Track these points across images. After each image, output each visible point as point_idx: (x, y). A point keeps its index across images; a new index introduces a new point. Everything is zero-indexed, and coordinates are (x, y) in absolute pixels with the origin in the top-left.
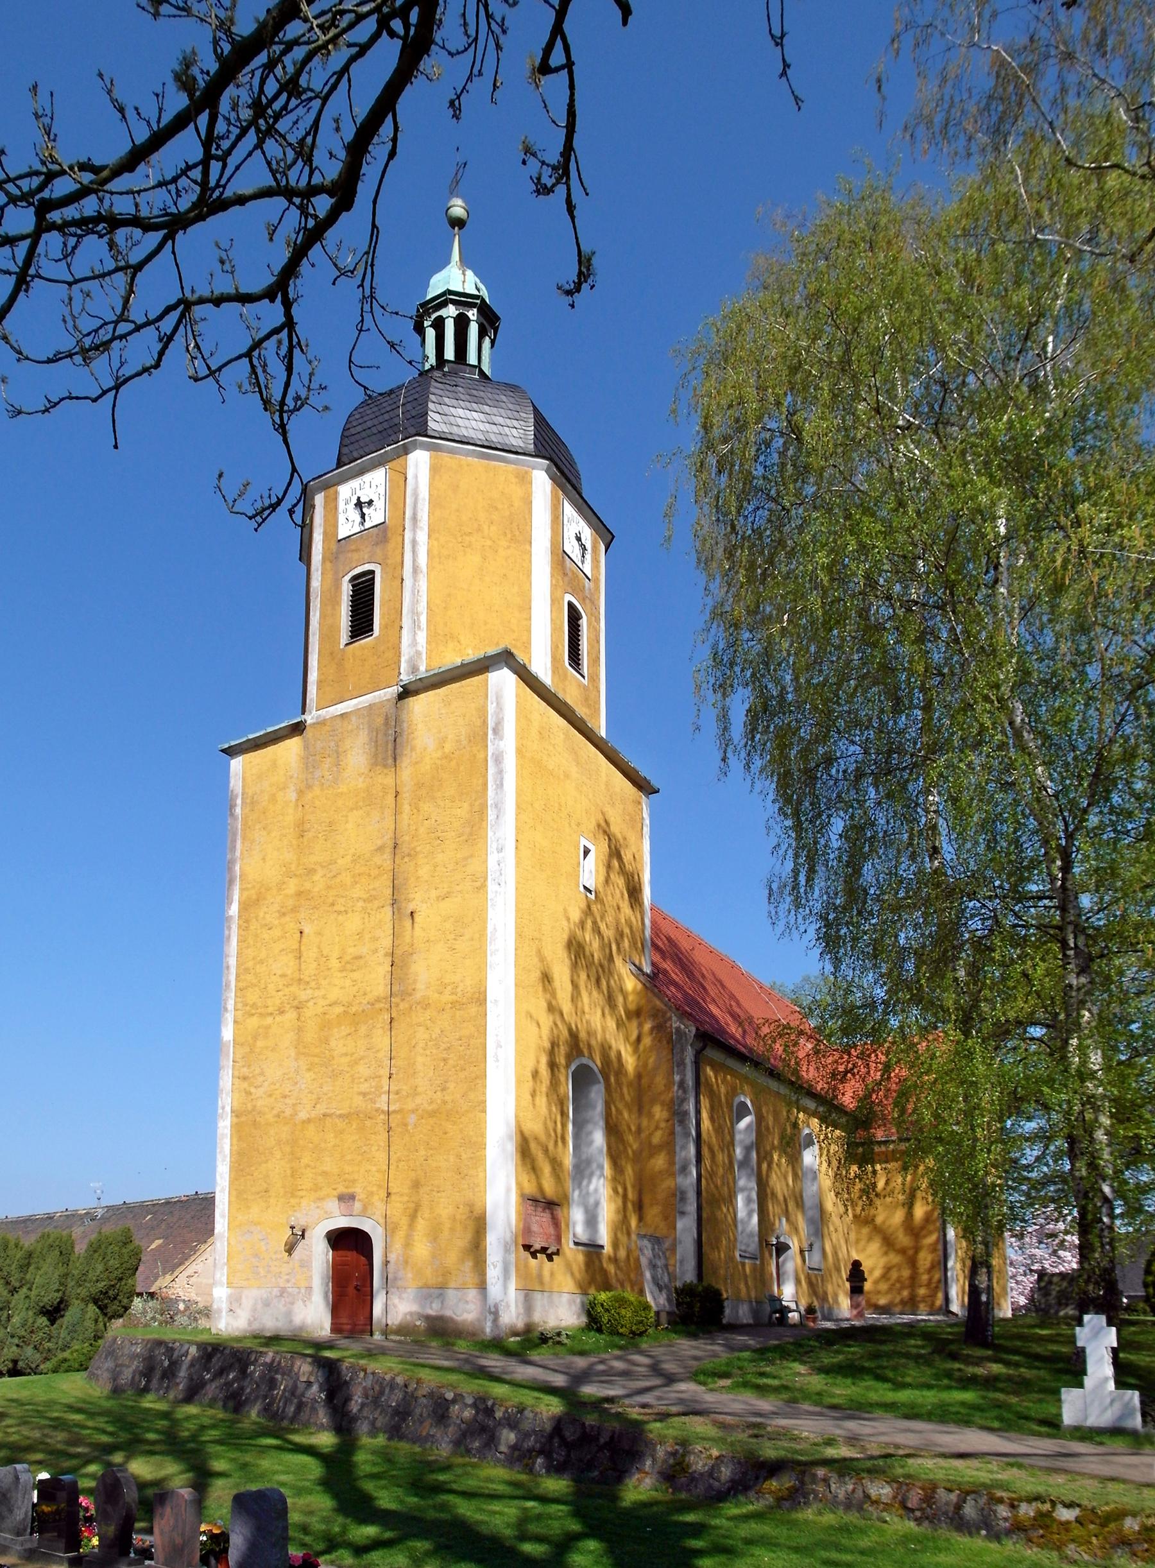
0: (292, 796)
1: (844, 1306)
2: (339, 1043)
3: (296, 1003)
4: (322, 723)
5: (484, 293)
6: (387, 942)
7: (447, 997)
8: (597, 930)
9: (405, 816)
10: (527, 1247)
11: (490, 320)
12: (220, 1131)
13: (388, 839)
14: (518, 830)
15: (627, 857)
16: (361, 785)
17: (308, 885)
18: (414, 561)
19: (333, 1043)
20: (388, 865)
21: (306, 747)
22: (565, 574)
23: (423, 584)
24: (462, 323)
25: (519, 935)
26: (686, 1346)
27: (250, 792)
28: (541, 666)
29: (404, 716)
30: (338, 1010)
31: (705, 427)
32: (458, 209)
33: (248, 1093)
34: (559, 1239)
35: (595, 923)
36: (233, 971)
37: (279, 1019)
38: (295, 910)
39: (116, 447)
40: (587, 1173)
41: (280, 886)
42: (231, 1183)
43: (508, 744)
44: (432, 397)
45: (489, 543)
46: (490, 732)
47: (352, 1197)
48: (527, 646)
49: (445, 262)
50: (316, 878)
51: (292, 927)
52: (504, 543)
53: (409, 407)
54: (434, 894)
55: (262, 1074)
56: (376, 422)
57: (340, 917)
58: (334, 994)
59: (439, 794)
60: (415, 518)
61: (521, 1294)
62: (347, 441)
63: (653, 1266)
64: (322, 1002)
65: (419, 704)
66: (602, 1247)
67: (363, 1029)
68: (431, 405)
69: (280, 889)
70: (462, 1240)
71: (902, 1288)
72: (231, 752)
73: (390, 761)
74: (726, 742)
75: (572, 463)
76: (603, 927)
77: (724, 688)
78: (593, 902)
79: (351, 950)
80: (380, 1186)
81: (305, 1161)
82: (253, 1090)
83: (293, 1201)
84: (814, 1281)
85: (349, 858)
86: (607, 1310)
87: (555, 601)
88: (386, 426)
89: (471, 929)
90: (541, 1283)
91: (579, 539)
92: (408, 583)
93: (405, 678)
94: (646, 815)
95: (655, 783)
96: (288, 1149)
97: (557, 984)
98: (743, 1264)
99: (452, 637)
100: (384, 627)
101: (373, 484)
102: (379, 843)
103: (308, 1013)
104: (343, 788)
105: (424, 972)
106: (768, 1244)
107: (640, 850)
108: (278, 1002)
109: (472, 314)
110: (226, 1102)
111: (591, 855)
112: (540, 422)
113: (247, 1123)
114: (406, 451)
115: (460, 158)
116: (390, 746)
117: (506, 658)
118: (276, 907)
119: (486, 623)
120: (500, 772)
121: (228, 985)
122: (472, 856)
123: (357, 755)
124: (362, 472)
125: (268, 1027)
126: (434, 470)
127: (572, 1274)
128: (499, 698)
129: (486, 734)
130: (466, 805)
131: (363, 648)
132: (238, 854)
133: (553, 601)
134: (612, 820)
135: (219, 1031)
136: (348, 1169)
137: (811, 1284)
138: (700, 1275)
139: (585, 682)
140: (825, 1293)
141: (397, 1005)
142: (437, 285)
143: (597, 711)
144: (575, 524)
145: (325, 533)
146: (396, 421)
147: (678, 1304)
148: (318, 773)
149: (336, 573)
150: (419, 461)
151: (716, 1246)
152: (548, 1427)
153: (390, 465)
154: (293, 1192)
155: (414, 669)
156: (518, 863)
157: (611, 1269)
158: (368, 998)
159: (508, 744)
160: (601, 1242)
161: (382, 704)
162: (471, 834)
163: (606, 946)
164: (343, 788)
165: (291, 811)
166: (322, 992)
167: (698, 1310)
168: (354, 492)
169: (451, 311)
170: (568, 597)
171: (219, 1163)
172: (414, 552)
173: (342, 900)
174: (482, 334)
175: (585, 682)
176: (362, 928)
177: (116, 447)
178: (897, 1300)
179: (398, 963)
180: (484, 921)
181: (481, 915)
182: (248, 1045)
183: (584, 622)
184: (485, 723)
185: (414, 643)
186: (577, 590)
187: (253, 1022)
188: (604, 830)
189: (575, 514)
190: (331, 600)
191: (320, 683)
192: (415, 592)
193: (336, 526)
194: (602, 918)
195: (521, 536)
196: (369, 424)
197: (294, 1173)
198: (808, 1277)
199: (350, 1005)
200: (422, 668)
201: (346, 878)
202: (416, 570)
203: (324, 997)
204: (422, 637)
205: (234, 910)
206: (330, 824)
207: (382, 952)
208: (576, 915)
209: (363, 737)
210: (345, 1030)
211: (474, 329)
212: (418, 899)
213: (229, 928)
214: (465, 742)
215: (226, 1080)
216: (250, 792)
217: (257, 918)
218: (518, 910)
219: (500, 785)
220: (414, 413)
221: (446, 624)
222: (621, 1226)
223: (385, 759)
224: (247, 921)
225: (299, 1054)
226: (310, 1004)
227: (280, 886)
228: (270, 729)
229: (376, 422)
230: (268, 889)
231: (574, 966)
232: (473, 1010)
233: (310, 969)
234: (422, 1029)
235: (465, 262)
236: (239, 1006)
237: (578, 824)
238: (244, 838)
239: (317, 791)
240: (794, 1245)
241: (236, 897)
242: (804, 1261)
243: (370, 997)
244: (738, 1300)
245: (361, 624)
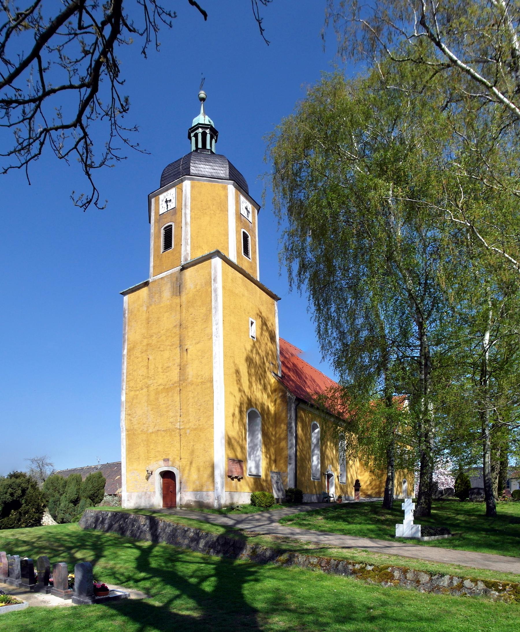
0: (145, 308)
1: (352, 495)
2: (162, 399)
3: (147, 385)
4: (154, 281)
5: (212, 123)
6: (178, 361)
7: (199, 380)
8: (258, 353)
9: (184, 314)
10: (229, 477)
11: (214, 133)
12: (122, 437)
13: (178, 323)
14: (224, 316)
15: (269, 324)
16: (168, 303)
17: (150, 342)
18: (186, 220)
19: (160, 400)
20: (178, 332)
21: (149, 291)
22: (241, 222)
23: (189, 229)
24: (204, 134)
25: (225, 356)
26: (286, 511)
27: (130, 308)
28: (233, 257)
29: (183, 277)
30: (162, 387)
31: (275, 164)
32: (202, 94)
33: (131, 420)
34: (242, 473)
35: (257, 350)
36: (125, 374)
37: (141, 392)
38: (146, 351)
39: (30, 184)
40: (256, 449)
41: (141, 342)
42: (126, 456)
43: (219, 285)
44: (191, 161)
45: (212, 212)
46: (212, 281)
47: (168, 460)
48: (227, 249)
49: (198, 113)
50: (153, 338)
51: (145, 357)
52: (218, 212)
53: (184, 165)
54: (194, 342)
55: (135, 413)
56: (172, 171)
57: (162, 353)
58: (160, 381)
59: (195, 305)
60: (185, 205)
61: (228, 493)
62: (163, 179)
63: (277, 483)
64: (156, 385)
65: (188, 272)
66: (260, 476)
67: (170, 394)
68: (191, 164)
69: (141, 343)
70: (206, 474)
71: (376, 488)
72: (124, 294)
73: (178, 294)
74: (291, 280)
75: (244, 181)
76: (260, 351)
77: (290, 259)
78: (256, 342)
79: (166, 365)
80: (178, 456)
81: (152, 447)
82: (132, 419)
83: (148, 462)
84: (343, 488)
85: (165, 330)
86: (257, 498)
87: (237, 232)
88: (175, 173)
89: (207, 354)
90: (237, 489)
91: (246, 209)
92: (183, 229)
93: (183, 263)
94: (276, 308)
95: (279, 296)
96: (145, 443)
97: (241, 373)
98: (314, 482)
99: (200, 247)
100: (176, 245)
101: (171, 194)
102: (175, 324)
103: (151, 389)
104: (162, 305)
105: (191, 372)
106: (324, 474)
107: (274, 321)
108: (141, 385)
109: (208, 131)
110: (123, 424)
111: (254, 325)
112: (232, 168)
113: (131, 434)
114: (182, 181)
115: (203, 77)
116: (178, 288)
117: (217, 253)
118: (140, 350)
119: (212, 241)
120: (216, 295)
121: (123, 380)
122: (207, 327)
123: (167, 293)
124: (167, 190)
125: (138, 395)
126: (192, 187)
127: (249, 486)
128: (215, 268)
129: (211, 282)
130: (205, 308)
131: (168, 253)
132: (126, 331)
133: (237, 232)
134: (262, 311)
135: (121, 397)
136: (166, 450)
137: (341, 488)
138: (296, 485)
139: (251, 260)
140: (347, 491)
141: (182, 384)
142: (195, 121)
143: (256, 271)
144: (245, 203)
145: (155, 213)
146: (179, 171)
147: (286, 496)
148: (154, 300)
149: (159, 227)
150: (187, 184)
151: (303, 474)
152: (215, 539)
153: (177, 186)
154: (148, 458)
155: (186, 259)
156: (224, 329)
157: (264, 484)
158: (172, 382)
159: (219, 285)
160: (260, 474)
161: (175, 273)
162: (207, 319)
163: (261, 358)
164: (162, 305)
165: (145, 314)
166: (155, 381)
167: (293, 498)
168: (165, 197)
169: (200, 130)
170: (243, 230)
171: (122, 448)
172: (185, 217)
173: (162, 346)
174: (211, 138)
175: (251, 260)
176: (170, 356)
177: (30, 184)
178: (374, 492)
179: (182, 368)
180: (212, 351)
181: (211, 349)
182: (131, 401)
183: (249, 239)
184: (211, 278)
185: (186, 250)
186: (246, 226)
187: (132, 393)
188: (260, 315)
189: (245, 200)
190: (157, 237)
191: (154, 266)
192: (186, 232)
193: (159, 210)
194: (260, 347)
195: (224, 209)
196: (170, 172)
197: (148, 452)
198: (340, 485)
199: (166, 385)
200: (189, 259)
201: (164, 338)
202: (186, 224)
203: (157, 383)
204: (189, 248)
205: (125, 352)
206: (158, 318)
207: (176, 365)
208: (249, 348)
209: (169, 285)
210: (164, 394)
211: (208, 137)
212: (189, 344)
213: (124, 359)
214: (204, 285)
215: (123, 416)
216: (130, 308)
217: (133, 354)
218: (224, 346)
219: (216, 300)
220: (185, 167)
221: (197, 243)
222: (269, 468)
223: (176, 293)
224: (130, 356)
225: (148, 404)
226: (152, 385)
227: (141, 342)
228: (137, 285)
229: (172, 171)
230: (137, 344)
231: (249, 367)
232: (209, 384)
233: (152, 372)
234: (191, 393)
235: (205, 113)
236: (127, 388)
237: (248, 313)
238: (129, 325)
239: (153, 306)
240: (335, 475)
241: (126, 347)
242: (339, 480)
243: (172, 382)
244: (312, 494)
245: (168, 244)
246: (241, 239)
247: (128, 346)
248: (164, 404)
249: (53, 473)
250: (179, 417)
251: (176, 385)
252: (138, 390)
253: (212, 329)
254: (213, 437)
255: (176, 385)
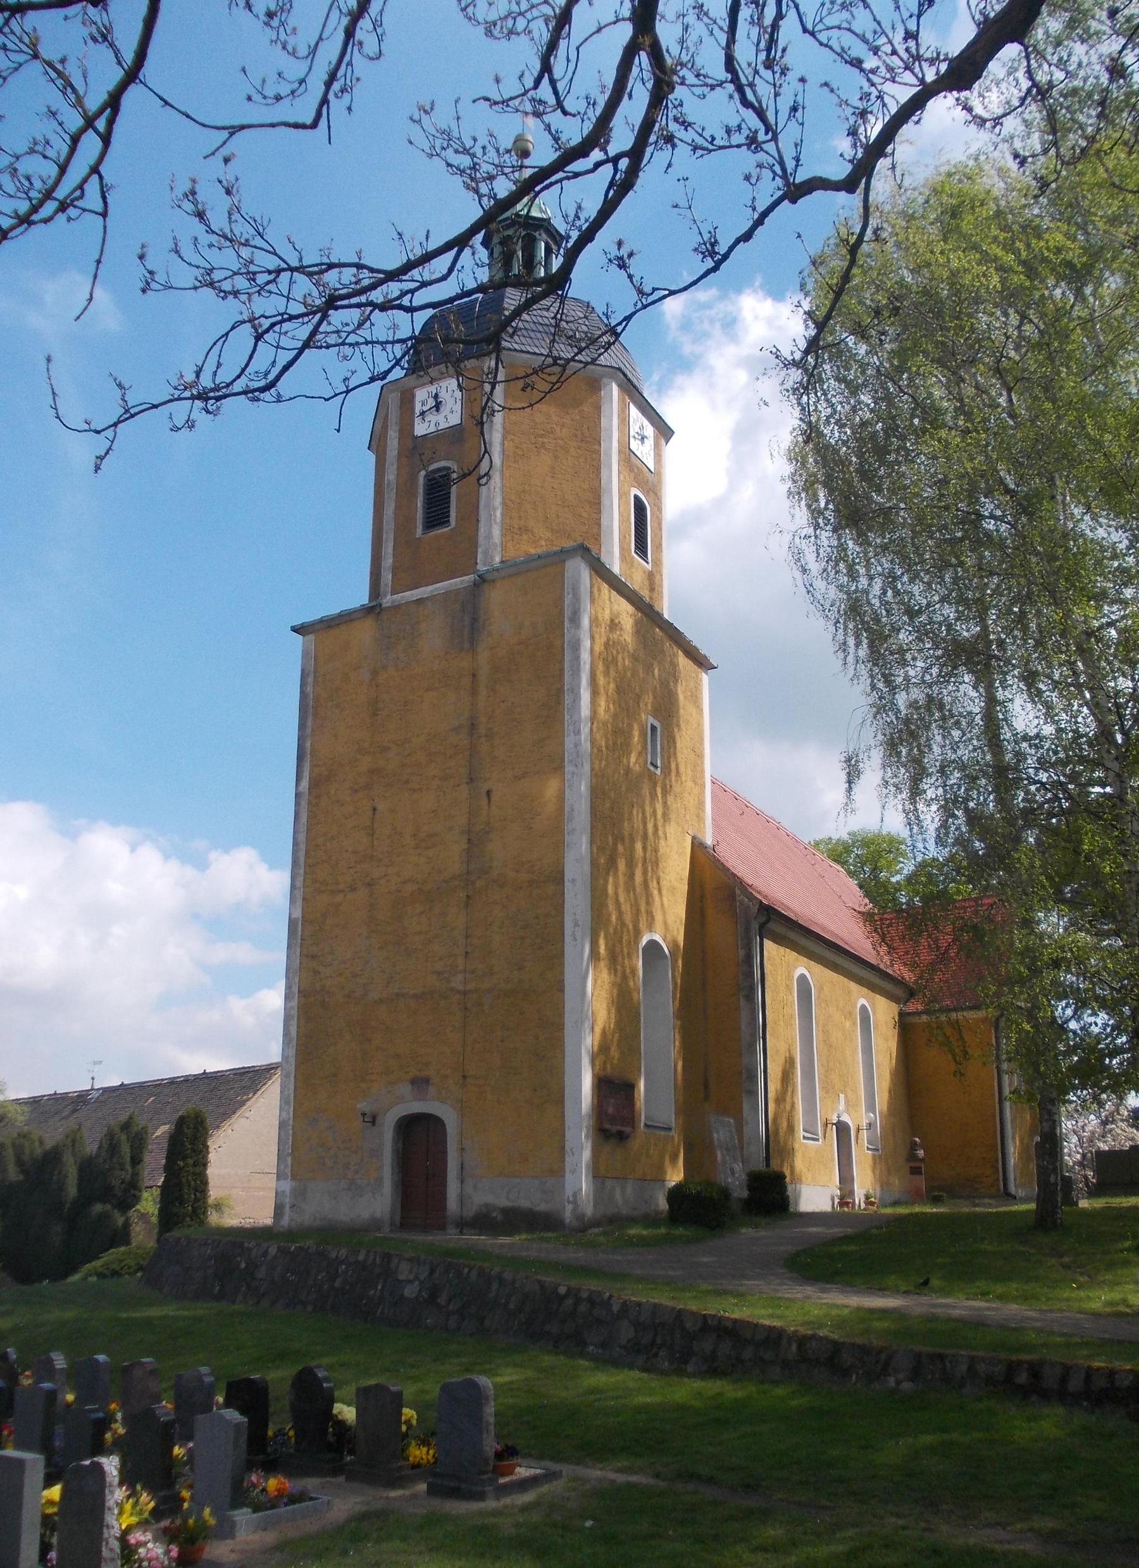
4: (396, 607)
73: (467, 645)
83: (363, 1085)
129: (563, 622)
161: (457, 592)
170: (635, 491)
184: (561, 612)
189: (640, 415)
224: (318, 797)
246: (629, 514)
247: (311, 771)
248: (420, 933)
249: (145, 1532)
250: (460, 961)
251: (457, 883)
252: (343, 891)
253: (562, 744)
254: (561, 1015)
255: (457, 883)
